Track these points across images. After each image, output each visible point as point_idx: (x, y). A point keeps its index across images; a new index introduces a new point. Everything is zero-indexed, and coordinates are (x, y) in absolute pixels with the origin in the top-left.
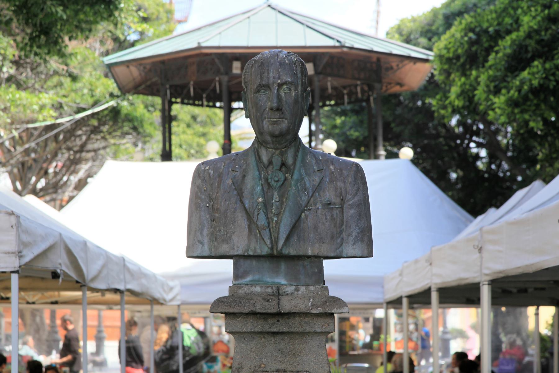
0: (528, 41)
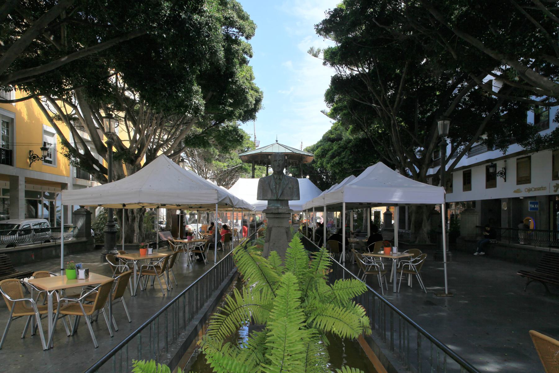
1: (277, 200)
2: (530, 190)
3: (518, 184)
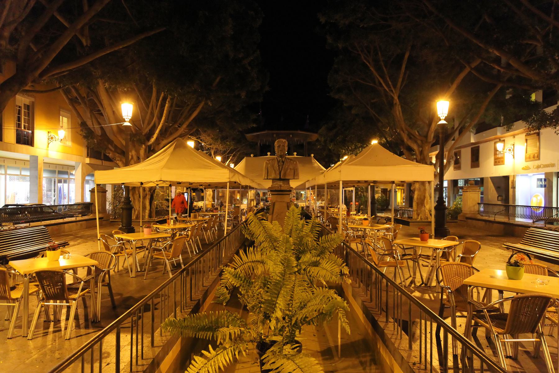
1: (280, 179)
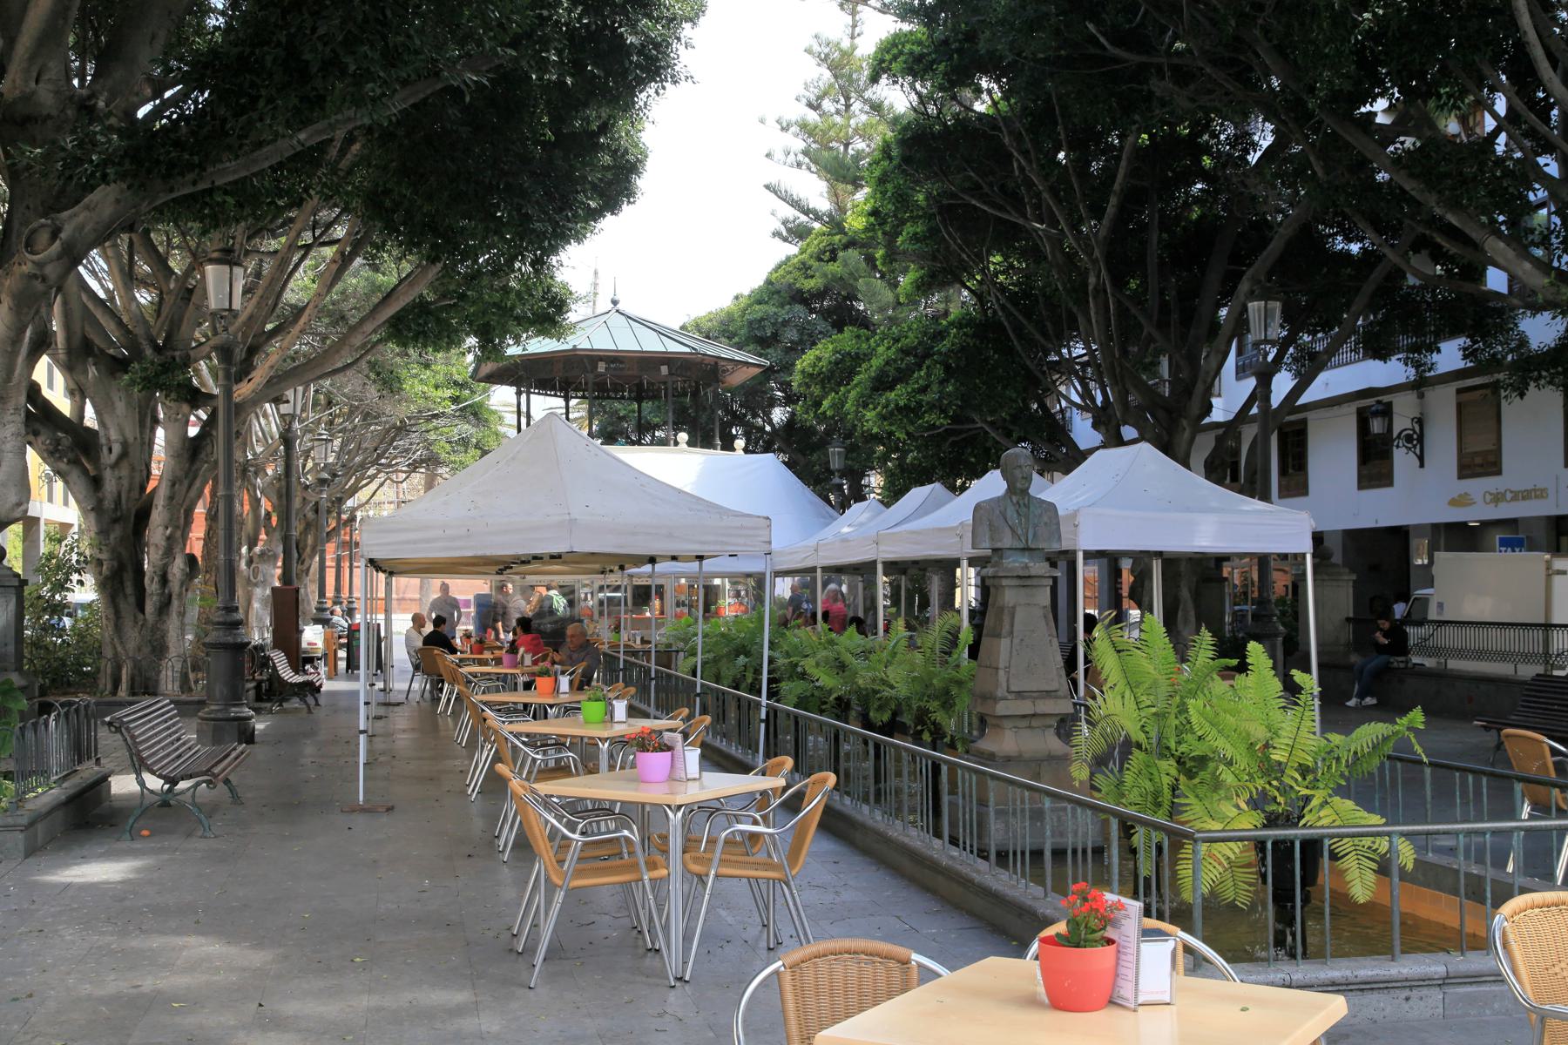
0: (888, 368)
2: (1497, 498)
3: (1461, 477)
